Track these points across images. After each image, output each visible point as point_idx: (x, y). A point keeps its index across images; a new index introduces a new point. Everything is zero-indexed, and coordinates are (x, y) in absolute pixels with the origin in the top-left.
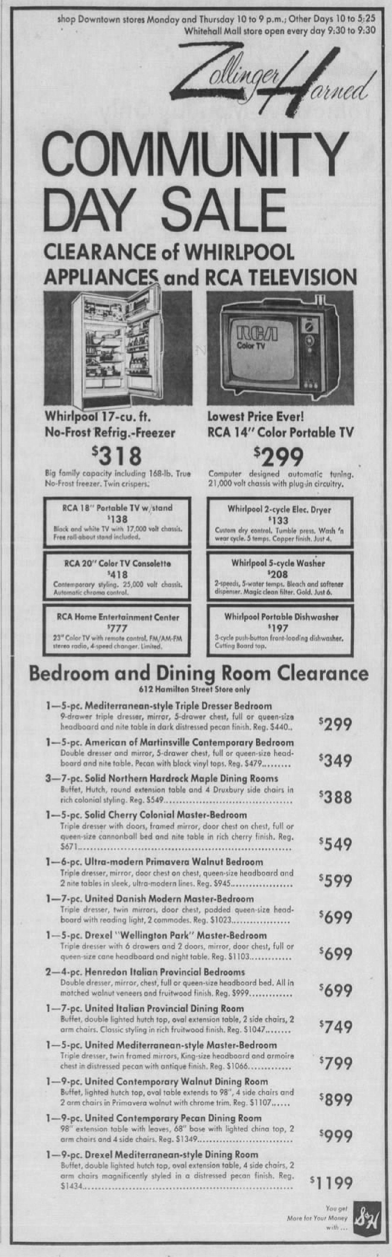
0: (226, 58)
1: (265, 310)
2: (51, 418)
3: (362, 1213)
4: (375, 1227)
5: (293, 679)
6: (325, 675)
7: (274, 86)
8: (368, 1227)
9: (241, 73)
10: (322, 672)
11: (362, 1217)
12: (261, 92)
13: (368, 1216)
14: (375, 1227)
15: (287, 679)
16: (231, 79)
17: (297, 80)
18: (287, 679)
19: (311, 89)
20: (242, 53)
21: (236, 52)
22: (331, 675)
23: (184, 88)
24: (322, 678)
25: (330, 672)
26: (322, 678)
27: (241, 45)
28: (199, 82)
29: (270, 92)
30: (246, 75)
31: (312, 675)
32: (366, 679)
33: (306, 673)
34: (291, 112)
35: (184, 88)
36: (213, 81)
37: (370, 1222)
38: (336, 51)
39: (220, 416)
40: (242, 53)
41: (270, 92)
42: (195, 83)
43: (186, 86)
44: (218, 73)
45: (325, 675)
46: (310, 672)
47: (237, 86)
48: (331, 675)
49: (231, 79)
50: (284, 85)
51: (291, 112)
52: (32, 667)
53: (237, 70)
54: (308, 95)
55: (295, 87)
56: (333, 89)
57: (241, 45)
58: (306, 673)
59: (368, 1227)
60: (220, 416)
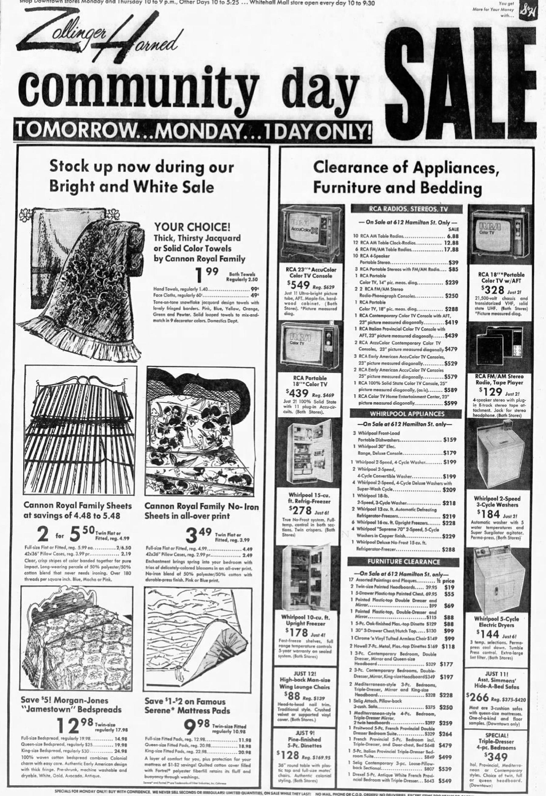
0: (67, 20)
1: (28, 444)
2: (141, 189)
3: (525, 7)
4: (534, 15)
5: (326, 171)
6: (352, 169)
7: (105, 41)
8: (529, 15)
9: (77, 31)
10: (350, 167)
11: (525, 9)
12: (95, 46)
13: (529, 9)
14: (534, 15)
15: (322, 171)
16: (69, 35)
17: (124, 36)
18: (322, 171)
19: (136, 44)
20: (79, 17)
21: (74, 16)
22: (358, 169)
23: (31, 40)
24: (350, 171)
25: (356, 166)
26: (350, 171)
27: (76, 10)
28: (45, 36)
29: (101, 46)
30: (81, 33)
31: (342, 169)
32: (379, 192)
33: (337, 167)
34: (119, 59)
35: (28, 41)
36: (55, 36)
37: (531, 12)
38: (155, 15)
39: (138, 165)
40: (79, 17)
41: (101, 46)
42: (36, 39)
43: (31, 40)
44: (59, 31)
45: (352, 169)
46: (340, 166)
47: (73, 41)
48: (358, 169)
49: (69, 35)
50: (113, 40)
51: (119, 59)
52: (51, 181)
53: (75, 29)
54: (133, 48)
55: (122, 42)
56: (151, 44)
57: (76, 10)
58: (337, 167)
59: (529, 15)
60: (138, 165)
